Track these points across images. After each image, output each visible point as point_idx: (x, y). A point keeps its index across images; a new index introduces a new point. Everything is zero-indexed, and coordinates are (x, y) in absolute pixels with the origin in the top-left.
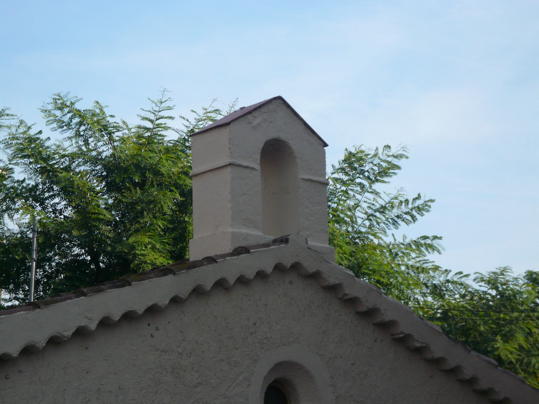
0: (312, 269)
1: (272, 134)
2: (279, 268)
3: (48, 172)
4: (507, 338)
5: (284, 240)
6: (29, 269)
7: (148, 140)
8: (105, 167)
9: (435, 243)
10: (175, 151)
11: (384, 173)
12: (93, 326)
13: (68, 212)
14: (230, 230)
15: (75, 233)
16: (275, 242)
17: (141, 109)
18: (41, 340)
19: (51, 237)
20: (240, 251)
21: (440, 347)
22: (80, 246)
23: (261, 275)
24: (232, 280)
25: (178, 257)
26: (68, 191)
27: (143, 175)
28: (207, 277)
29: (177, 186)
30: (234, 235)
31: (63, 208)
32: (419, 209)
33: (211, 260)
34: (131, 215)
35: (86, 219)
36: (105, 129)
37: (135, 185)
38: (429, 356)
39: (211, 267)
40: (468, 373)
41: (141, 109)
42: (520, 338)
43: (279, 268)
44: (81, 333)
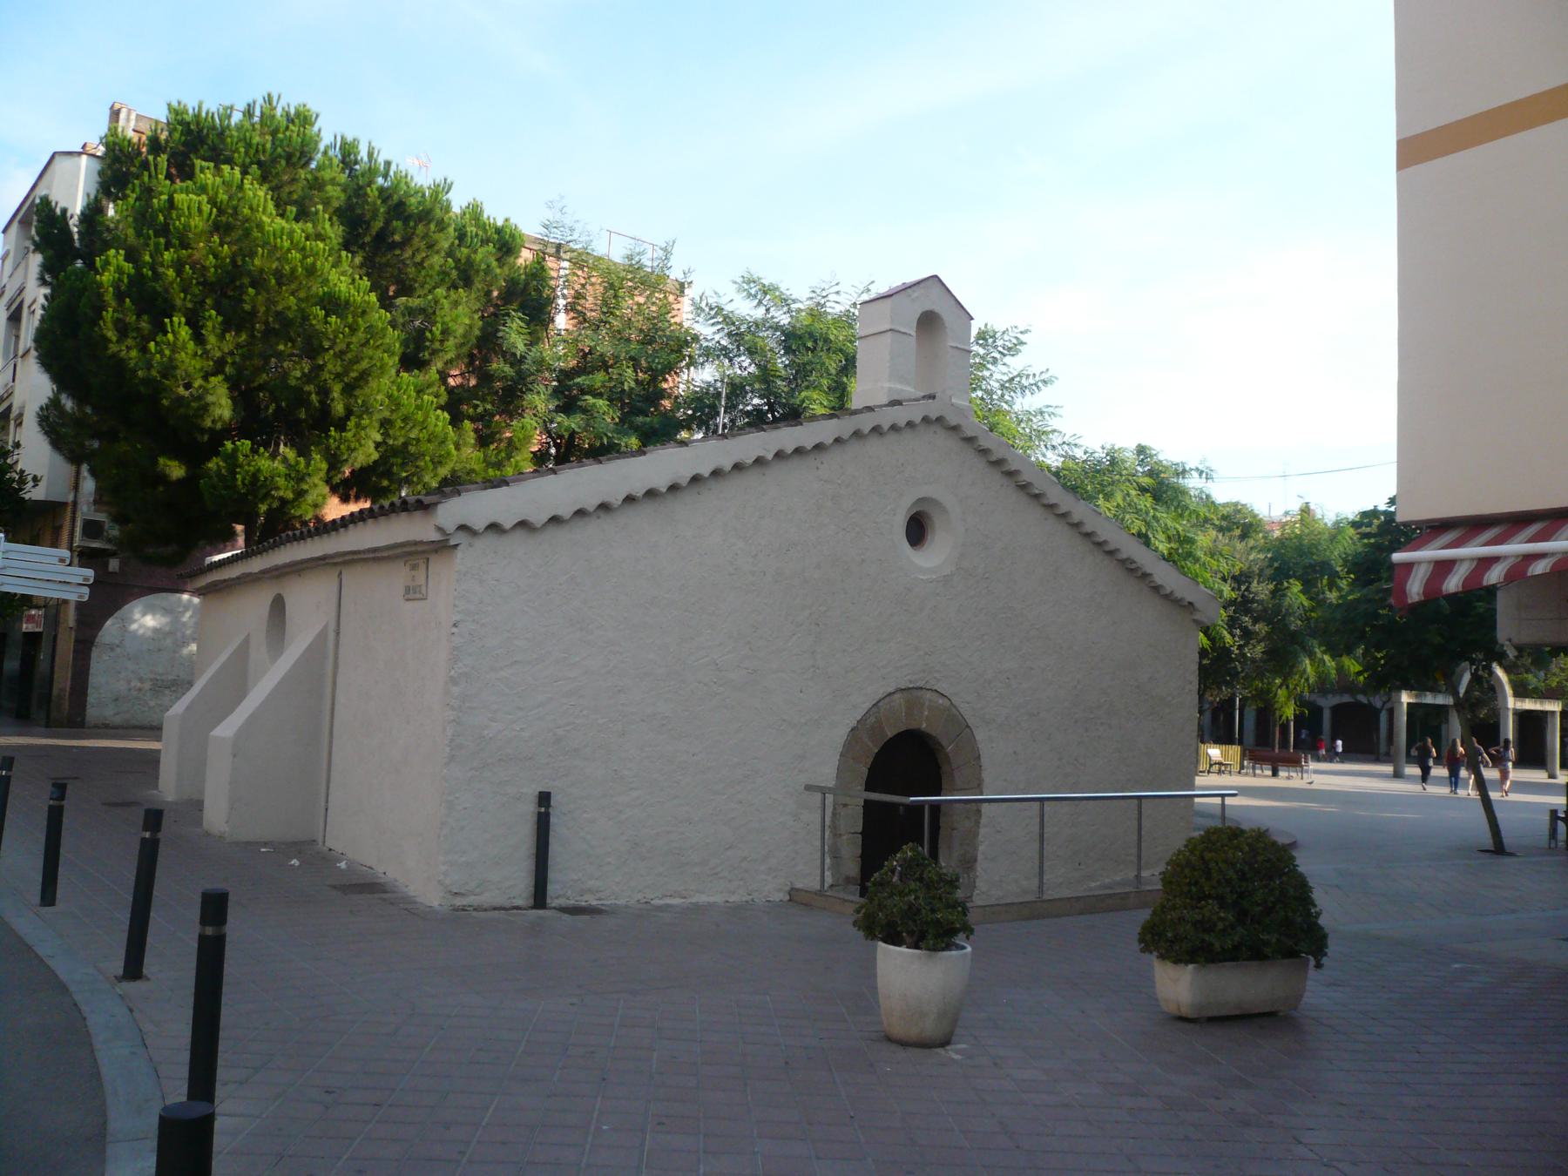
0: (953, 423)
1: (927, 307)
2: (926, 420)
3: (736, 337)
4: (1108, 497)
5: (932, 397)
6: (718, 414)
7: (816, 313)
8: (783, 333)
9: (1057, 411)
10: (846, 320)
11: (1012, 350)
12: (770, 456)
13: (752, 369)
14: (887, 385)
15: (757, 386)
16: (924, 397)
17: (544, 798)
18: (727, 465)
19: (737, 389)
20: (895, 403)
21: (1055, 494)
22: (761, 397)
23: (910, 424)
24: (886, 427)
25: (840, 408)
26: (751, 352)
27: (815, 341)
28: (866, 423)
29: (841, 350)
30: (890, 389)
31: (745, 366)
32: (1045, 382)
33: (870, 409)
34: (801, 374)
35: (766, 375)
36: (785, 301)
37: (808, 349)
38: (1045, 502)
39: (869, 414)
40: (1076, 518)
41: (544, 798)
42: (1119, 498)
43: (926, 420)
44: (759, 461)
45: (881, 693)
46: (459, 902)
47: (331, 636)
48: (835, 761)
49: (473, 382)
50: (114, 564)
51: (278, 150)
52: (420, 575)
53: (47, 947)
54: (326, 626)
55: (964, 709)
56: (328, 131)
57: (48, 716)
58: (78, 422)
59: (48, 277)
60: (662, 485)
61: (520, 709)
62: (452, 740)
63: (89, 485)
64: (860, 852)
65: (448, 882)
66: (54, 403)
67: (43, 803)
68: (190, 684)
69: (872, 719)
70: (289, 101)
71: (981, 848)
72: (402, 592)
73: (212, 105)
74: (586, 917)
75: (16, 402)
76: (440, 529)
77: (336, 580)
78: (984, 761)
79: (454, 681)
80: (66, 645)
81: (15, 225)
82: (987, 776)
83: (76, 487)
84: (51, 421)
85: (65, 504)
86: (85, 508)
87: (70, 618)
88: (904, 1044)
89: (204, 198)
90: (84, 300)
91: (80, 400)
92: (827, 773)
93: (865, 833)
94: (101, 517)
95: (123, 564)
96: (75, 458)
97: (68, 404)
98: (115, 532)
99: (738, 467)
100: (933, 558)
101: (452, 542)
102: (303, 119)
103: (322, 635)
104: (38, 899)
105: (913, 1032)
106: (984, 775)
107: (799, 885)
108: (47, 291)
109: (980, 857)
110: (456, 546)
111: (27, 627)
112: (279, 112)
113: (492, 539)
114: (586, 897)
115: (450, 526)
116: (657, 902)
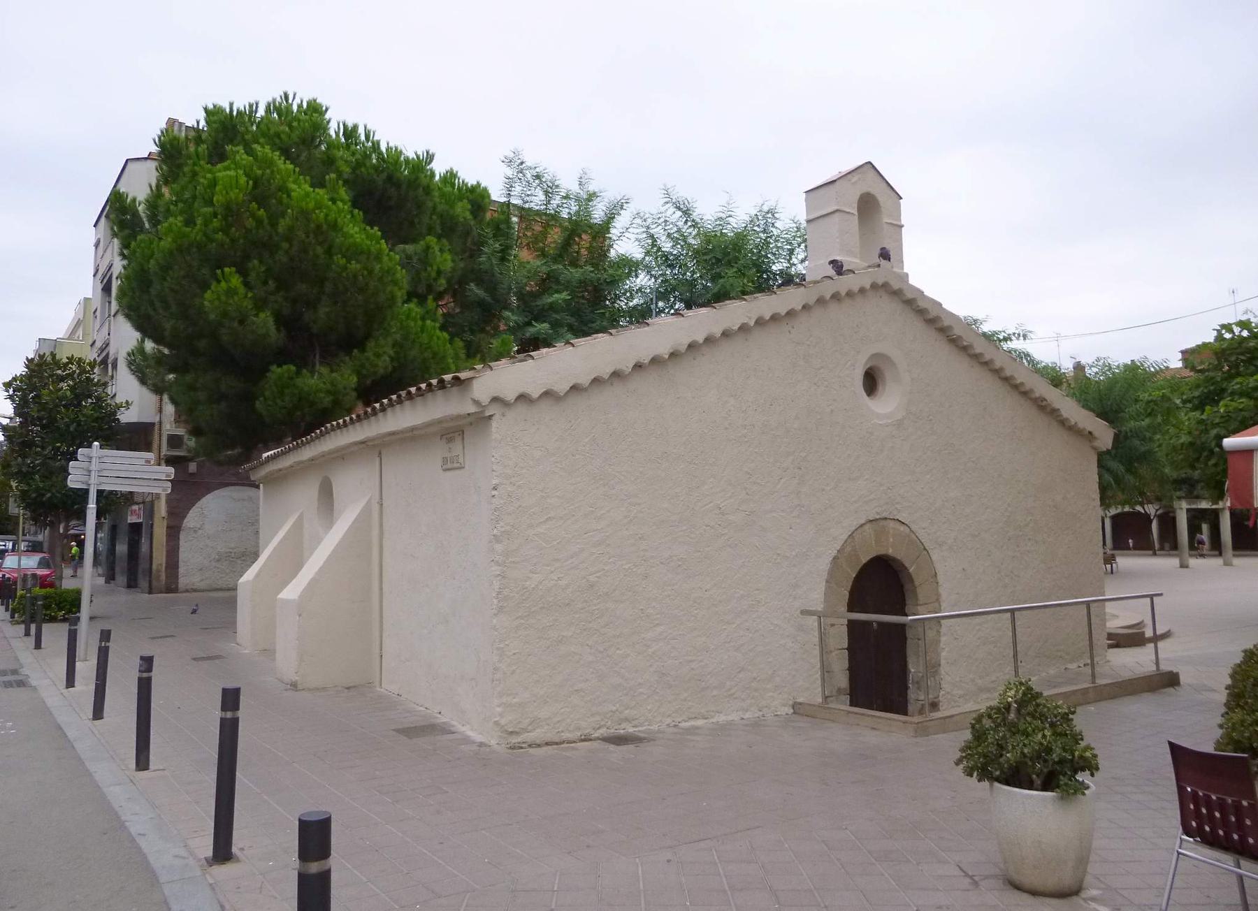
1: (865, 189)
18: (717, 331)
23: (862, 291)
44: (744, 328)
45: (856, 524)
46: (515, 740)
47: (376, 507)
48: (822, 586)
49: (458, 310)
50: (193, 467)
51: (297, 133)
52: (457, 447)
53: (138, 820)
54: (369, 502)
55: (922, 535)
56: (336, 118)
57: (150, 586)
58: (159, 360)
59: (125, 252)
60: (664, 351)
61: (558, 560)
62: (499, 593)
63: (169, 409)
64: (847, 665)
65: (503, 722)
66: (140, 349)
67: (134, 675)
68: (256, 556)
69: (848, 549)
70: (302, 95)
71: (943, 654)
72: (440, 463)
73: (241, 104)
74: (631, 747)
75: (112, 350)
76: (476, 402)
77: (378, 460)
78: (940, 578)
79: (497, 539)
80: (160, 531)
81: (103, 219)
82: (944, 591)
83: (160, 411)
84: (141, 367)
85: (153, 424)
86: (168, 427)
87: (162, 509)
88: (1034, 893)
89: (241, 172)
90: (152, 262)
91: (158, 340)
92: (816, 597)
93: (850, 649)
94: (181, 431)
95: (199, 466)
96: (158, 390)
97: (149, 345)
98: (191, 442)
99: (726, 334)
100: (887, 405)
101: (487, 414)
102: (315, 109)
103: (366, 511)
104: (134, 766)
105: (1051, 883)
106: (941, 590)
107: (800, 700)
108: (125, 262)
109: (943, 662)
110: (491, 416)
111: (132, 519)
112: (295, 108)
113: (522, 409)
114: (623, 726)
115: (485, 399)
116: (683, 725)
